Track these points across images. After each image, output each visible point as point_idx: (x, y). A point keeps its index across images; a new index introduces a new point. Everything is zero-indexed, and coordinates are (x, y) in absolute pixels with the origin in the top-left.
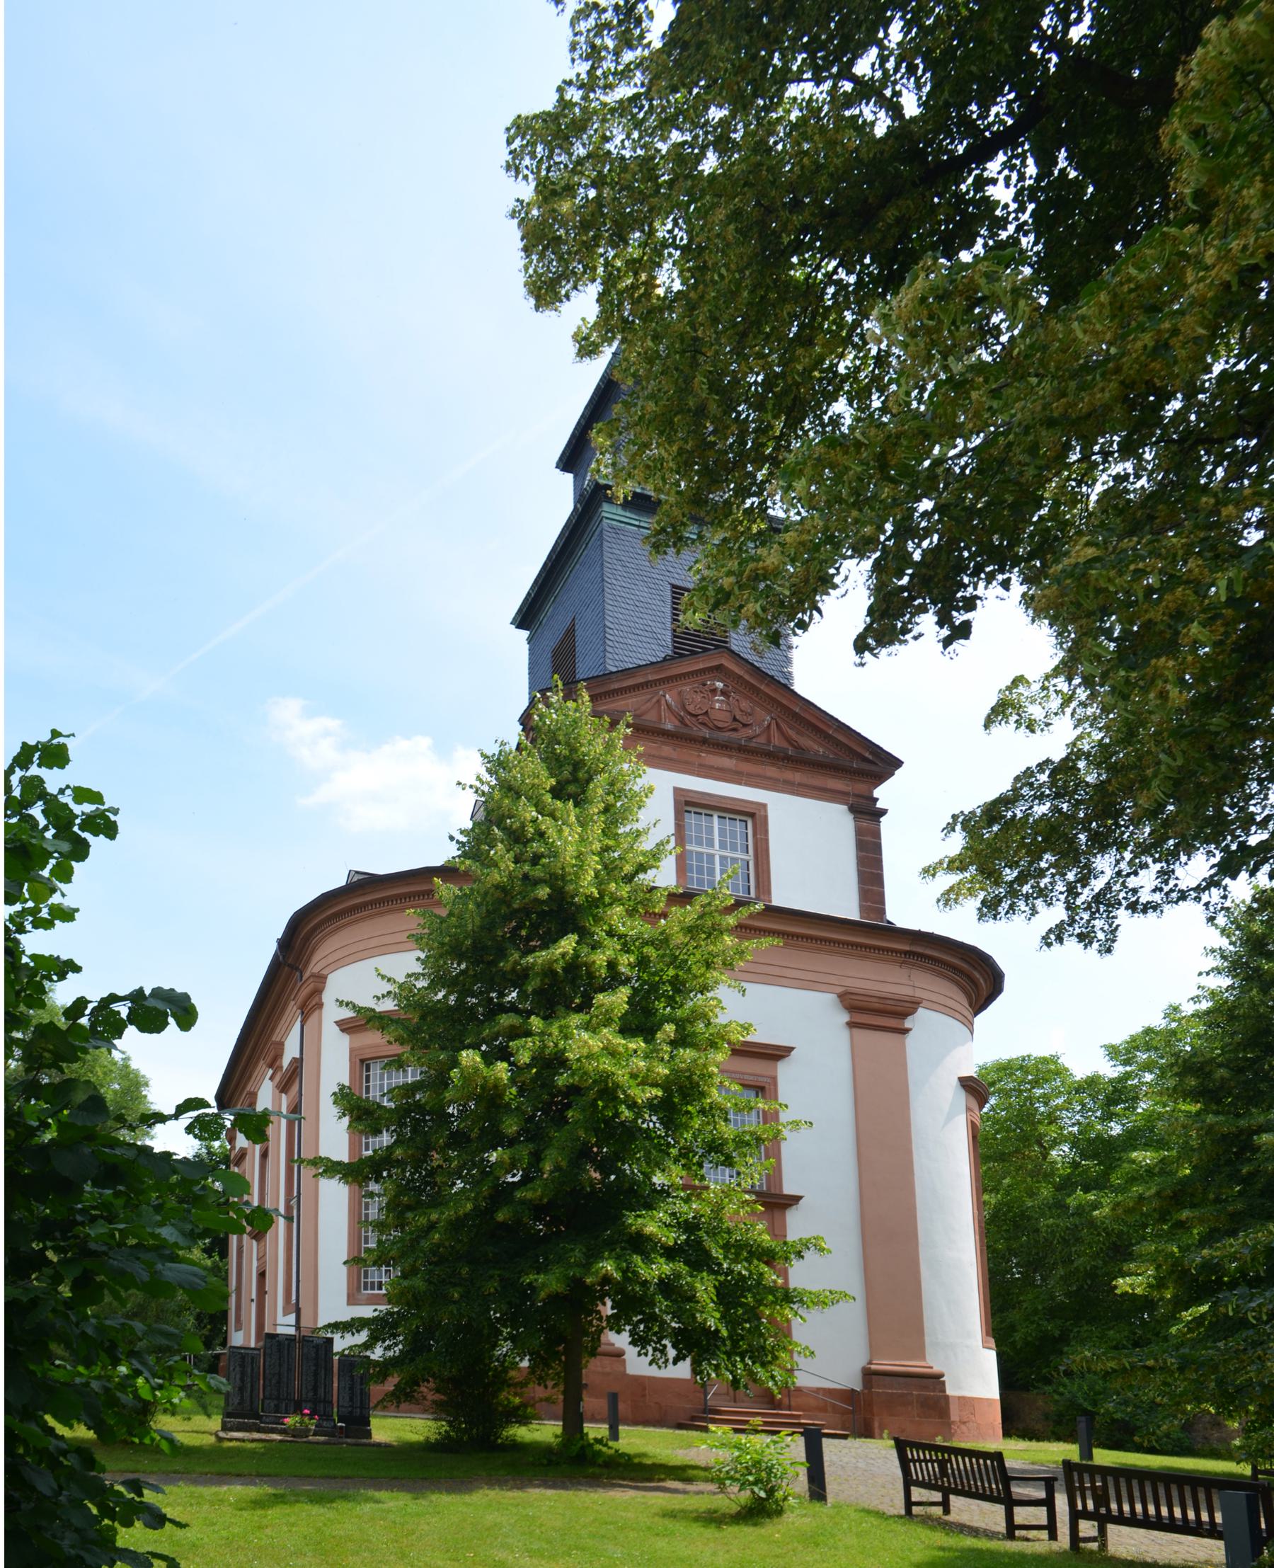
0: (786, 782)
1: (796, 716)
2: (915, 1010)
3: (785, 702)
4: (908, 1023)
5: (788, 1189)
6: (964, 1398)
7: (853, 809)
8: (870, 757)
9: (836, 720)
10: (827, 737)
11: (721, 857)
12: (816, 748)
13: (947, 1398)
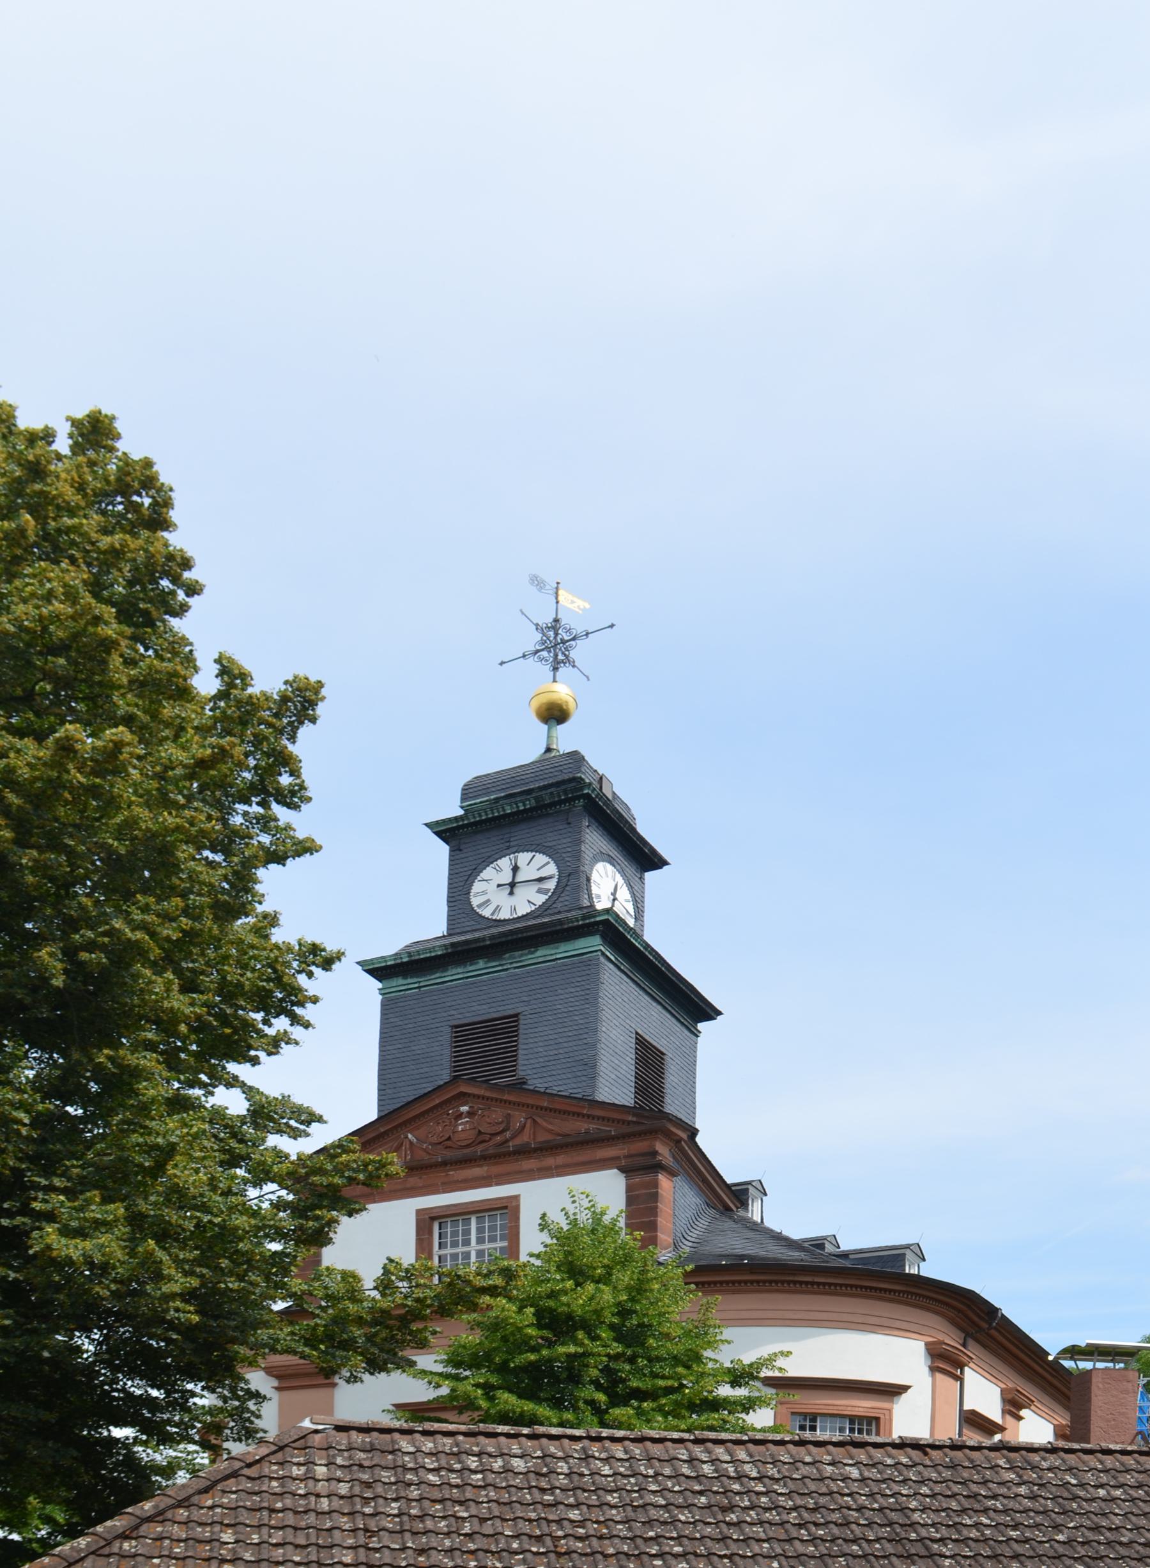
7: (622, 1170)
8: (634, 1119)
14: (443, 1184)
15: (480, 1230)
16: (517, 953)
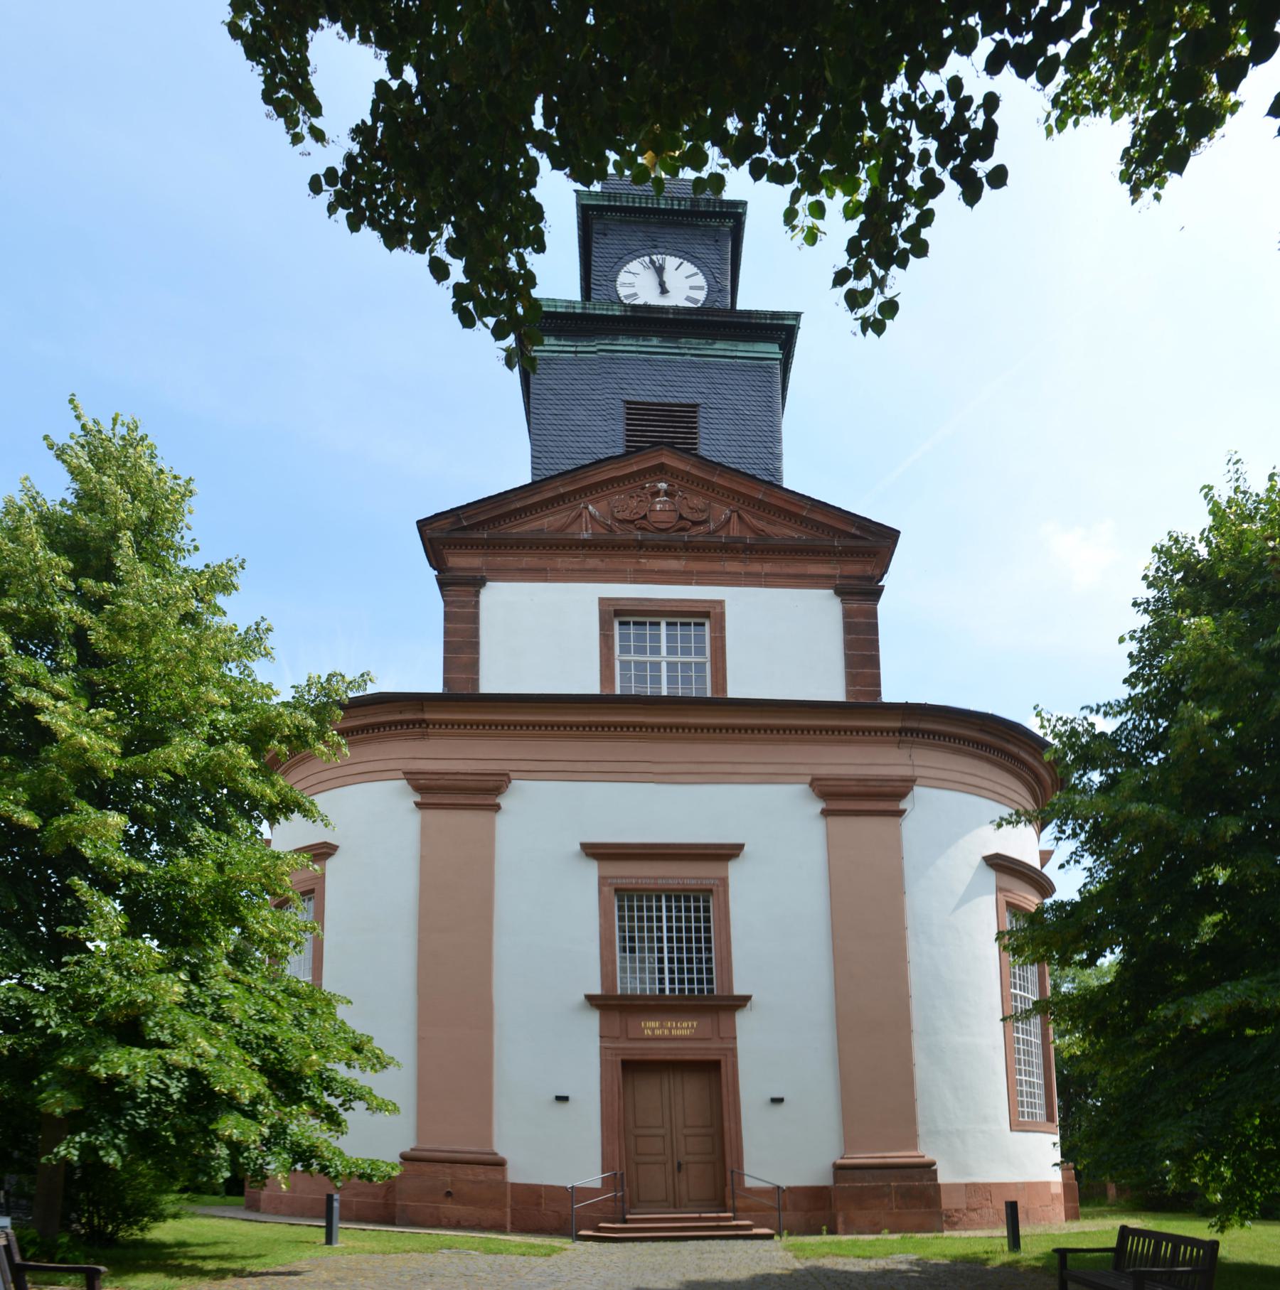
0: (748, 574)
1: (760, 504)
2: (910, 789)
3: (743, 490)
4: (903, 805)
5: (738, 991)
6: (974, 1185)
7: (841, 592)
8: (858, 533)
9: (809, 498)
10: (804, 521)
11: (668, 663)
12: (784, 532)
13: (937, 1187)
14: (636, 571)
15: (671, 638)
16: (694, 341)
